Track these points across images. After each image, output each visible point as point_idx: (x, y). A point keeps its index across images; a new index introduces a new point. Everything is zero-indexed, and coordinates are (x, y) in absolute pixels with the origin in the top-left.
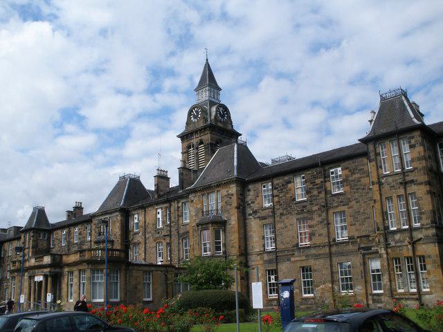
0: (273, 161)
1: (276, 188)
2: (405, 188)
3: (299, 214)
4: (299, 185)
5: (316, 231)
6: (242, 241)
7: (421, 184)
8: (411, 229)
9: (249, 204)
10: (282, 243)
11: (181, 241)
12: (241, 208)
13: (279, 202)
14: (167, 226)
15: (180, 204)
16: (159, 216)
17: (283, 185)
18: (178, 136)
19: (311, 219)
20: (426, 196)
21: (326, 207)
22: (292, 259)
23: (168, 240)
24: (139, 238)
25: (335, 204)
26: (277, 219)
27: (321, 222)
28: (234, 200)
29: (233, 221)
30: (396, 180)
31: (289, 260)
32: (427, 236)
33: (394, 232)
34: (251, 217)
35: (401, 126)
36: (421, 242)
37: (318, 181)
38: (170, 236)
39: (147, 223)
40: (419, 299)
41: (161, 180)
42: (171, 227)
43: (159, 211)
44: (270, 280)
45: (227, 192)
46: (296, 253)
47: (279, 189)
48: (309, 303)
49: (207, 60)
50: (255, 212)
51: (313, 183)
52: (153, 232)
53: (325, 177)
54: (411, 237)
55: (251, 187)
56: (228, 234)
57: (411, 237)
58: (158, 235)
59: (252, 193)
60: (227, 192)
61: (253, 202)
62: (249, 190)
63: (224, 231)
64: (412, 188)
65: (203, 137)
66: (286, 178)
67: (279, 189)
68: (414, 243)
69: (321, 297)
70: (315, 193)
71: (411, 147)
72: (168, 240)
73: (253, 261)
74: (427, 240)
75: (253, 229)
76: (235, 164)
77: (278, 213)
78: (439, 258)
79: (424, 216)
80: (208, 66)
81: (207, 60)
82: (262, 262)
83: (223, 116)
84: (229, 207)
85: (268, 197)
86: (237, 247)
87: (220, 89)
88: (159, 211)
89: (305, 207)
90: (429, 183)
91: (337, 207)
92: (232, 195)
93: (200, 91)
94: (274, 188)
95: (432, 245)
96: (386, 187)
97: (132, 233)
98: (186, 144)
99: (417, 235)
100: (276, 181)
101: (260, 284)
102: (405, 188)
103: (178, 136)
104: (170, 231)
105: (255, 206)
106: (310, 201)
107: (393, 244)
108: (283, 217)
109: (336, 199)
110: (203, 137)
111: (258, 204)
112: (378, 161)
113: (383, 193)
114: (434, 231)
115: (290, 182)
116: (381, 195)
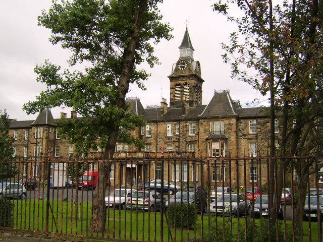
0: (147, 107)
1: (259, 124)
11: (187, 145)
14: (177, 135)
15: (187, 124)
16: (169, 129)
18: (169, 77)
23: (177, 144)
28: (234, 127)
29: (233, 138)
35: (187, 196)
38: (179, 142)
39: (158, 132)
42: (179, 136)
49: (187, 30)
50: (244, 135)
55: (242, 121)
58: (169, 140)
61: (244, 130)
62: (241, 123)
63: (226, 143)
65: (188, 81)
66: (266, 120)
72: (177, 144)
81: (187, 30)
84: (229, 131)
85: (253, 128)
88: (170, 125)
92: (233, 124)
94: (258, 124)
98: (174, 83)
100: (259, 120)
101: (266, 166)
104: (179, 139)
105: (245, 132)
110: (188, 81)
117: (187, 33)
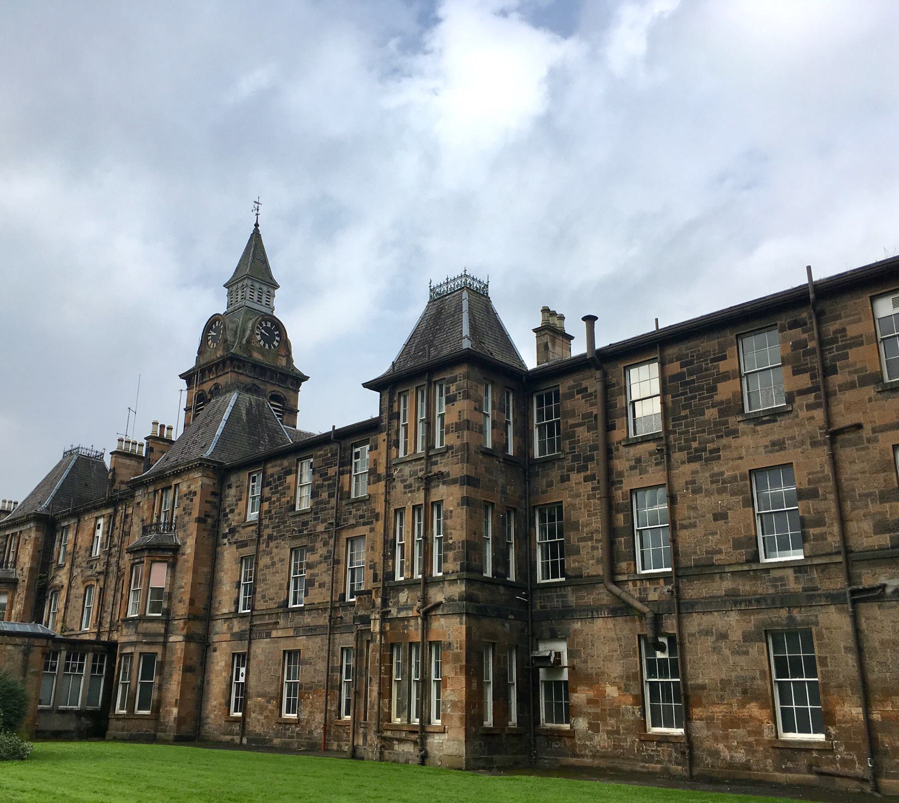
2: (427, 490)
3: (294, 538)
4: (307, 478)
5: (317, 575)
6: (202, 589)
7: (454, 481)
8: (428, 582)
9: (226, 515)
10: (263, 597)
12: (209, 520)
13: (270, 512)
16: (99, 533)
17: (279, 478)
18: (182, 376)
19: (312, 550)
20: (459, 510)
21: (338, 526)
22: (274, 634)
24: (62, 578)
25: (352, 521)
26: (263, 547)
27: (326, 558)
30: (415, 473)
31: (268, 635)
32: (450, 600)
33: (400, 586)
34: (225, 541)
36: (439, 612)
37: (332, 471)
38: (106, 573)
40: (422, 744)
41: (121, 460)
43: (101, 521)
44: (237, 679)
45: (189, 487)
46: (282, 622)
47: (273, 485)
48: (289, 733)
49: (257, 225)
50: (233, 531)
51: (323, 475)
52: (84, 565)
53: (342, 464)
54: (425, 599)
56: (178, 575)
57: (425, 599)
59: (233, 491)
60: (189, 487)
62: (230, 487)
64: (440, 492)
66: (286, 463)
67: (273, 485)
68: (428, 613)
69: (308, 722)
70: (325, 495)
71: (450, 400)
73: (217, 633)
74: (450, 607)
75: (225, 567)
76: (219, 432)
77: (266, 532)
78: (464, 652)
79: (451, 554)
80: (256, 236)
81: (257, 225)
82: (228, 637)
83: (268, 340)
86: (187, 602)
87: (275, 286)
89: (305, 524)
90: (468, 481)
91: (353, 526)
92: (195, 493)
93: (234, 288)
95: (455, 620)
96: (399, 486)
97: (54, 566)
99: (437, 595)
102: (427, 490)
103: (182, 376)
106: (316, 513)
107: (394, 612)
108: (272, 544)
109: (354, 511)
111: (239, 514)
112: (393, 432)
113: (392, 499)
114: (463, 588)
115: (289, 472)
116: (387, 501)
117: (256, 236)
